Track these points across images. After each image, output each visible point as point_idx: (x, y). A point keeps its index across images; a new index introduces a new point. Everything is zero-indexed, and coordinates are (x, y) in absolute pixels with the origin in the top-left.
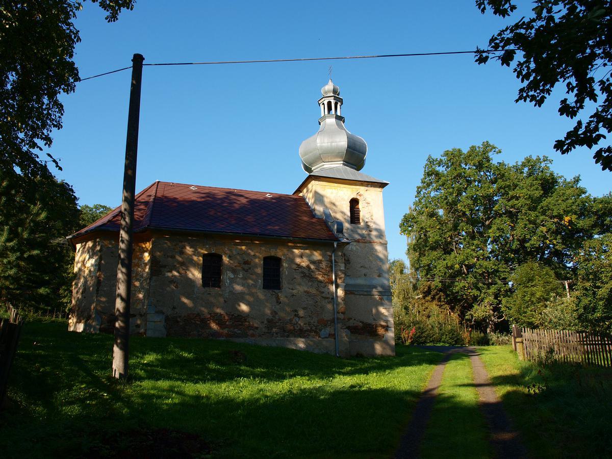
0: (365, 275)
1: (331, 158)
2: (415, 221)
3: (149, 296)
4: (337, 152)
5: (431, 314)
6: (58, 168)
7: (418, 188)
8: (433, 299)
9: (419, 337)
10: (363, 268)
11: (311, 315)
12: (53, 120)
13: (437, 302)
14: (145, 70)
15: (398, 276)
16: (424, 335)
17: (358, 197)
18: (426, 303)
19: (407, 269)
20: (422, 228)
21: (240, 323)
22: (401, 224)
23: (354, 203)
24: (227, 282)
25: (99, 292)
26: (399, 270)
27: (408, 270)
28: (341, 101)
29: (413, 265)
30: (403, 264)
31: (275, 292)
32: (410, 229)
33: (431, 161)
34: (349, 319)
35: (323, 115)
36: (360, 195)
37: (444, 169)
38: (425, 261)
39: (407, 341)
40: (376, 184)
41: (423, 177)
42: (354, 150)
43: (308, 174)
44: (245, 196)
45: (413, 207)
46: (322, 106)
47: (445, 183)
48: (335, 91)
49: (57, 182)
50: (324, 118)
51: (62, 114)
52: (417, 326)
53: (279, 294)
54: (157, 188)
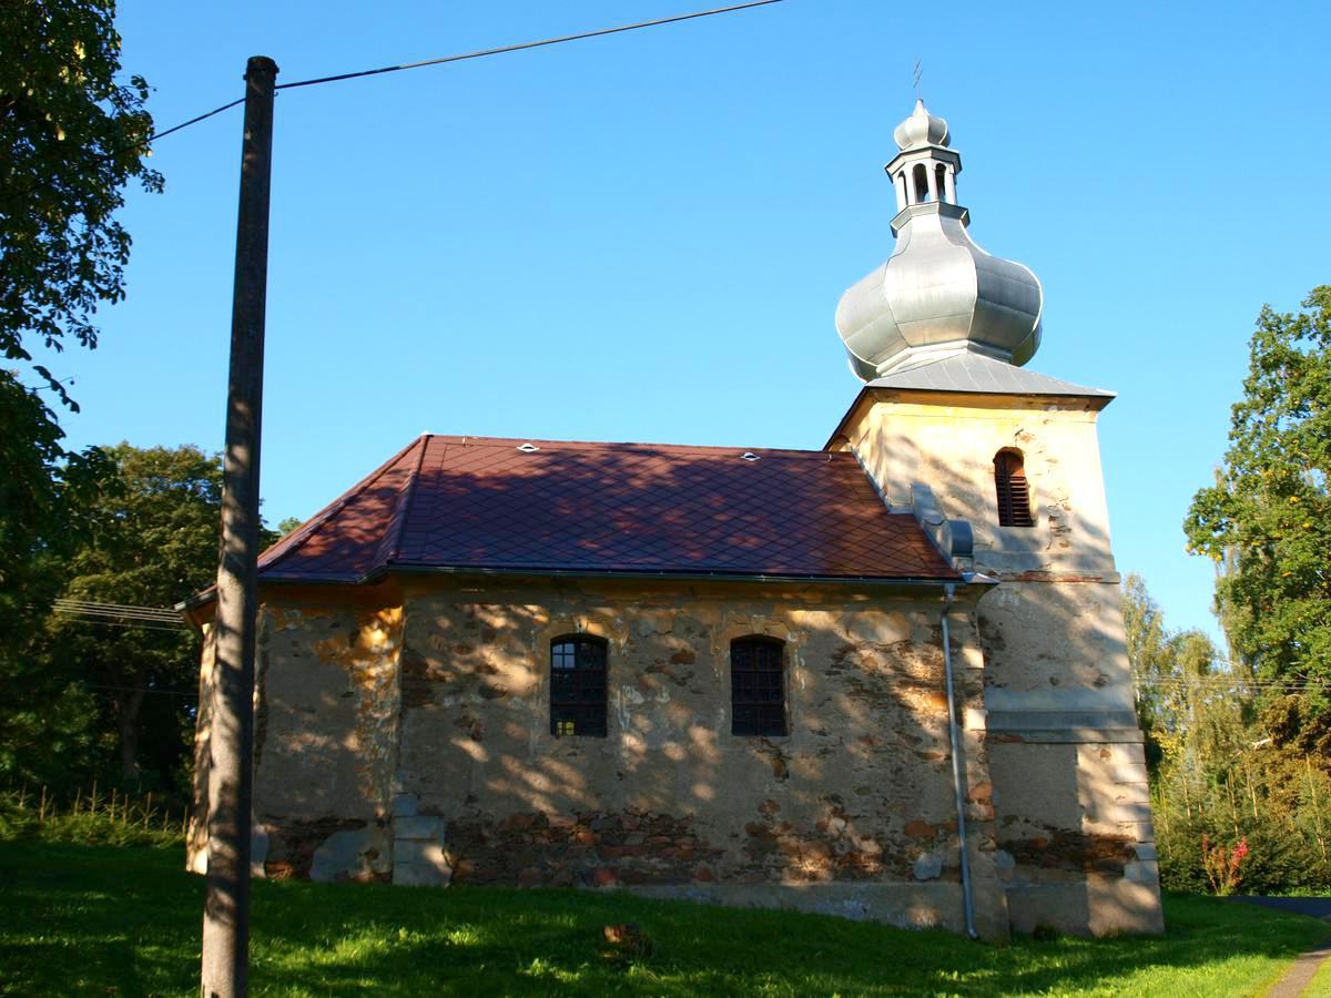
0: (1054, 682)
1: (931, 335)
2: (1232, 510)
3: (398, 765)
4: (949, 311)
5: (1302, 796)
6: (69, 404)
7: (1237, 409)
8: (1308, 747)
9: (1264, 869)
10: (1045, 660)
11: (882, 809)
12: (100, 278)
13: (1318, 759)
14: (282, 103)
15: (1194, 679)
16: (1277, 862)
17: (1021, 445)
18: (1287, 762)
19: (1222, 658)
20: (1255, 531)
21: (668, 840)
22: (1187, 522)
23: (1008, 461)
24: (624, 719)
25: (263, 757)
26: (1194, 662)
27: (1225, 661)
28: (956, 161)
29: (1237, 647)
30: (1207, 645)
31: (769, 744)
32: (1217, 535)
33: (1272, 325)
34: (1009, 820)
35: (901, 205)
36: (1026, 439)
37: (1314, 345)
38: (1273, 631)
39: (1224, 881)
40: (1074, 400)
41: (1250, 374)
42: (1000, 303)
43: (864, 383)
44: (48, 383)
45: (1227, 469)
46: (898, 182)
47: (1319, 388)
48: (934, 134)
49: (204, 458)
50: (905, 216)
51: (125, 262)
52: (1255, 834)
53: (783, 747)
54: (423, 455)
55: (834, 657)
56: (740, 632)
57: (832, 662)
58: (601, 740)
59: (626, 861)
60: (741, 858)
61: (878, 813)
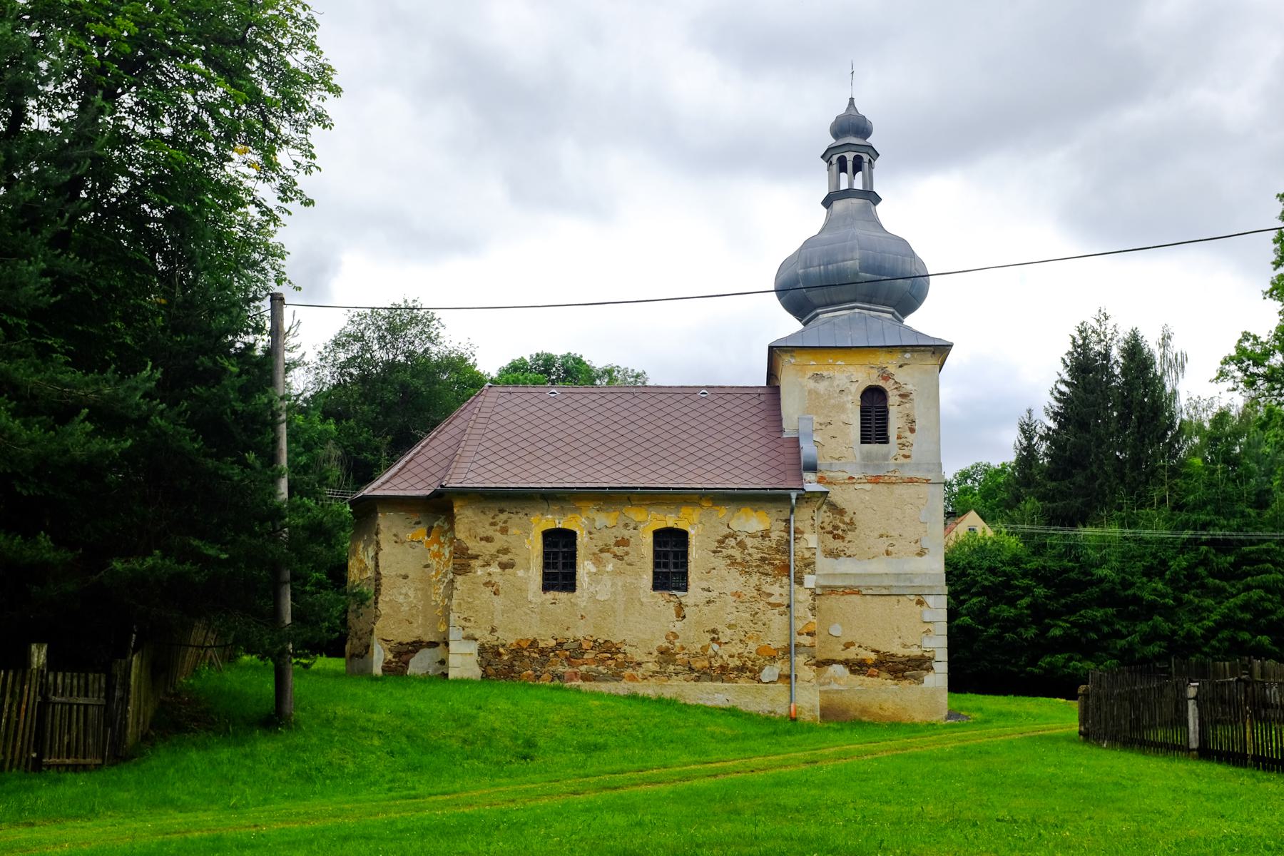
11: (743, 638)
21: (609, 655)
55: (719, 542)
56: (661, 525)
57: (716, 544)
58: (570, 595)
59: (583, 668)
60: (653, 667)
61: (741, 640)
